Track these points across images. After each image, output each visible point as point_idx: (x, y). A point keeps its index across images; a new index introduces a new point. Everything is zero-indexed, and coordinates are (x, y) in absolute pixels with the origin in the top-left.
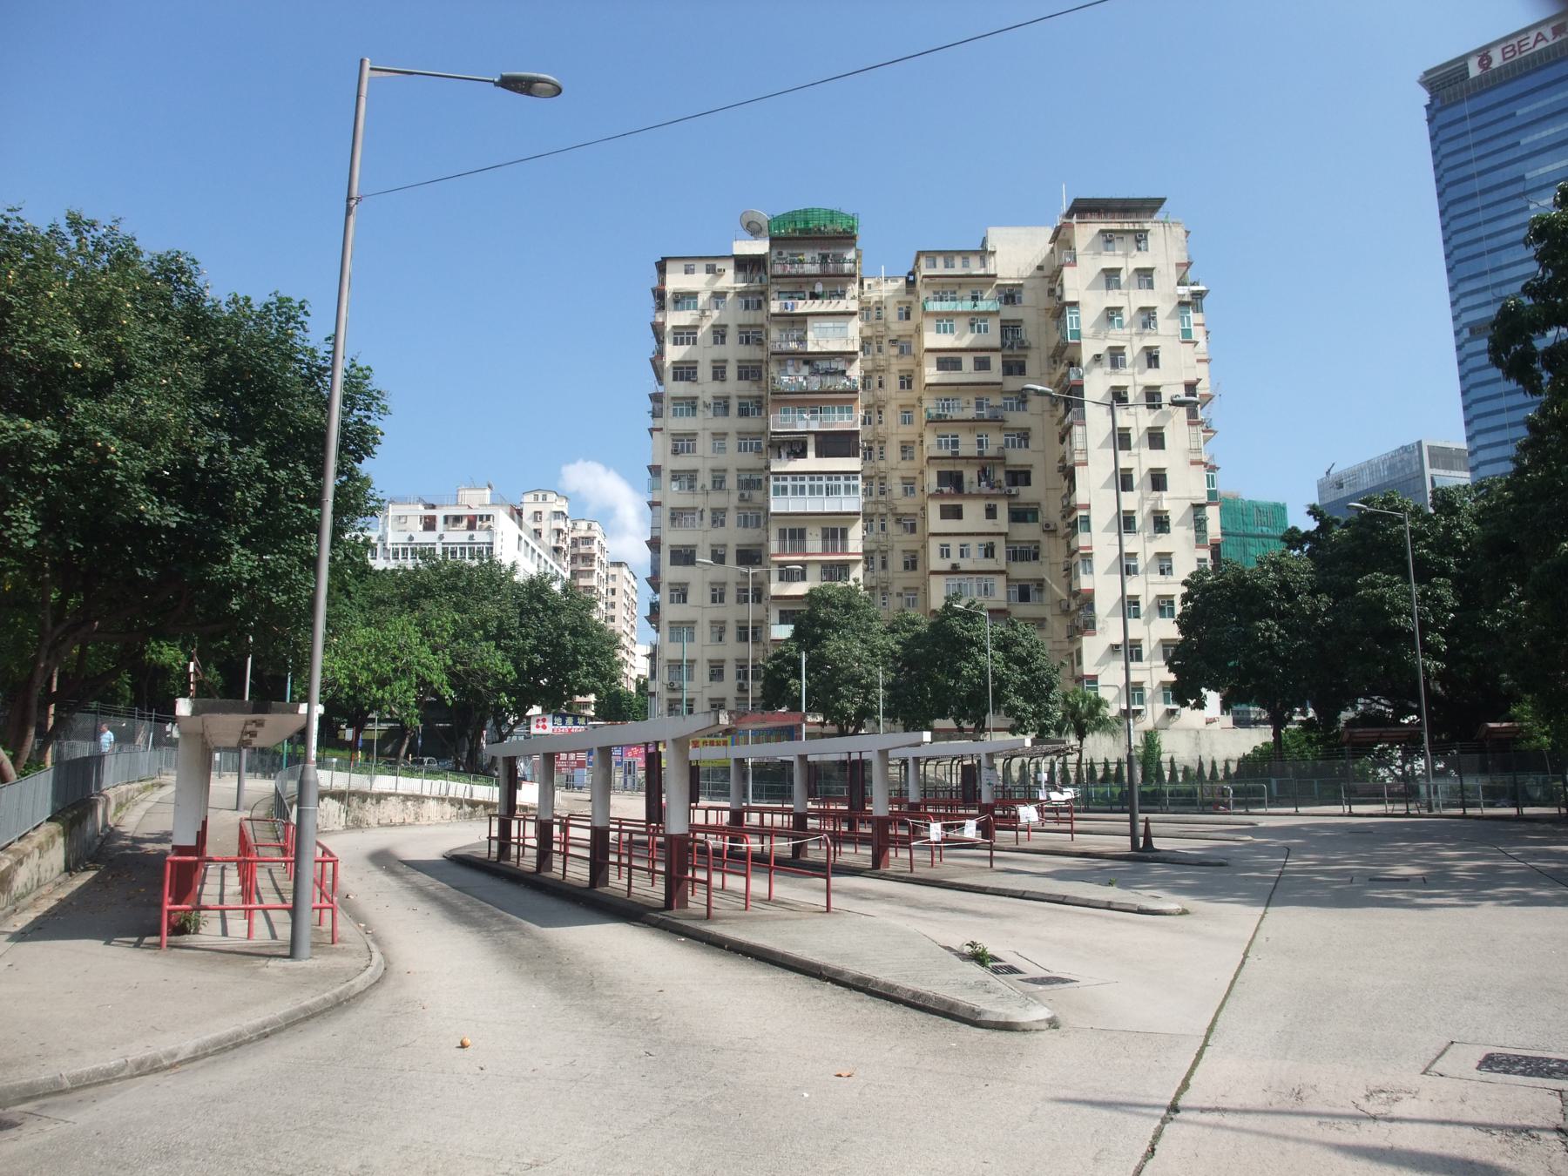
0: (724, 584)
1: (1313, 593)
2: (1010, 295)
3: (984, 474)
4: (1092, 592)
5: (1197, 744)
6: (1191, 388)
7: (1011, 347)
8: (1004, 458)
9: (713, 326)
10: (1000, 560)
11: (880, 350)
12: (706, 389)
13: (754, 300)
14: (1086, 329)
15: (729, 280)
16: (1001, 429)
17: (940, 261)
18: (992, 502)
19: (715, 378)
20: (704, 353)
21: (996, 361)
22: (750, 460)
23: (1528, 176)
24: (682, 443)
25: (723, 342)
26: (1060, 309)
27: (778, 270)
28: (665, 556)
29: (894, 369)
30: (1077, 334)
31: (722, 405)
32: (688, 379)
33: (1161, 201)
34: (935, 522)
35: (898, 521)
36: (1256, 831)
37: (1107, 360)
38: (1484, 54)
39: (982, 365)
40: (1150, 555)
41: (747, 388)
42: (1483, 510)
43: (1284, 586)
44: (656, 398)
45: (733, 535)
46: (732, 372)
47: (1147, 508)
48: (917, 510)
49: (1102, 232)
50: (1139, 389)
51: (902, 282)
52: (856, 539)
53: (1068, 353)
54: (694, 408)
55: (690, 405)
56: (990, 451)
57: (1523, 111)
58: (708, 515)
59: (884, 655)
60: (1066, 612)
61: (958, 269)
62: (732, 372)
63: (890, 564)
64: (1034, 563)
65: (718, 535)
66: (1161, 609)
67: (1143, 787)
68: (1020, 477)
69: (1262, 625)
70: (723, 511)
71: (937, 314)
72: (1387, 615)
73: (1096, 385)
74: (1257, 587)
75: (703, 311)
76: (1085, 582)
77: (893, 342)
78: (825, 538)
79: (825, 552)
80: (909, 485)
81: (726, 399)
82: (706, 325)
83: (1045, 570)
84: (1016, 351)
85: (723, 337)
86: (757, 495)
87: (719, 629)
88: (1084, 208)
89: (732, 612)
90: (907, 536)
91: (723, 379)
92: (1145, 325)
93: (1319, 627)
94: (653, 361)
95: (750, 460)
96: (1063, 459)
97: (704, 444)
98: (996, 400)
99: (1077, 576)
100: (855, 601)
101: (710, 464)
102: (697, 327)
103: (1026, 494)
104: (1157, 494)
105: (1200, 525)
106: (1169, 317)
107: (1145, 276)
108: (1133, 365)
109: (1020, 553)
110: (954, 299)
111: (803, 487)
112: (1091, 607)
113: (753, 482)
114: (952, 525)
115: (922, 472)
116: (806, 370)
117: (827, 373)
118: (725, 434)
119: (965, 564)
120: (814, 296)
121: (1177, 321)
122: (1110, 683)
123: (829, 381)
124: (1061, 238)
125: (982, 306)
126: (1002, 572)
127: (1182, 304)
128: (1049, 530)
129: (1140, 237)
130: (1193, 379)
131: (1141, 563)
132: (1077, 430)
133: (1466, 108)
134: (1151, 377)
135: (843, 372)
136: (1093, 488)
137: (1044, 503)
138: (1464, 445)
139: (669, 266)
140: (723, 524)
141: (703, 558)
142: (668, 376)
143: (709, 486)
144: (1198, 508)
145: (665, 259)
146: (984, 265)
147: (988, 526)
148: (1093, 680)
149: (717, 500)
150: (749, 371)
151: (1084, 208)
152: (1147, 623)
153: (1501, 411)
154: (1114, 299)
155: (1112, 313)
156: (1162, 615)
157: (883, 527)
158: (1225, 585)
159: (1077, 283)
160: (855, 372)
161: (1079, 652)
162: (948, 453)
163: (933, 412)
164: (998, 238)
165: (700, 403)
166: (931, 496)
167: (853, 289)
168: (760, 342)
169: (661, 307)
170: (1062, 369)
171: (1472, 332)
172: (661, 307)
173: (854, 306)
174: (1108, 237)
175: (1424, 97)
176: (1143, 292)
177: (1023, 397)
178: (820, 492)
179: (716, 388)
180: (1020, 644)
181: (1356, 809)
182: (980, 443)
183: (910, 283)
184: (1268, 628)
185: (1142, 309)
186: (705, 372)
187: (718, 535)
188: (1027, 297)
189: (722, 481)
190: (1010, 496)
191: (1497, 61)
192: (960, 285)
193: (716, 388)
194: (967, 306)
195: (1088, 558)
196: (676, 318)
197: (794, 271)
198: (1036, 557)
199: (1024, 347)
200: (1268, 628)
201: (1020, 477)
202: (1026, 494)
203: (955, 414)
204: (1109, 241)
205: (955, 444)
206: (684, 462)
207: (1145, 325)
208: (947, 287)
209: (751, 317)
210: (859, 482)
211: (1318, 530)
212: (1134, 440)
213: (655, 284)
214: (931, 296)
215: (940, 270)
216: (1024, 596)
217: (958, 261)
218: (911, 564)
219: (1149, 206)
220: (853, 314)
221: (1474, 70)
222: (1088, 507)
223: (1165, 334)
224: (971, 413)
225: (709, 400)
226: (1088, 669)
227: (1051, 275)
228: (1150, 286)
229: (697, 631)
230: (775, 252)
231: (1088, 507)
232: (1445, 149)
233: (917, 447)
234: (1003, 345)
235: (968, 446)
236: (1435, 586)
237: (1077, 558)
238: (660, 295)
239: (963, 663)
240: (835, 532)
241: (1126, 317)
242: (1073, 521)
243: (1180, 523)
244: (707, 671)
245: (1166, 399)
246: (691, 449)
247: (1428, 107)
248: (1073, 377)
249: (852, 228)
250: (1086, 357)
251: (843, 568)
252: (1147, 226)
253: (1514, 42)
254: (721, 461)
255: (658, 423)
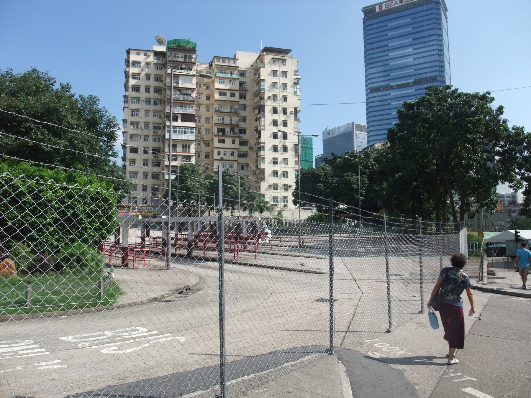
0: (148, 160)
1: (332, 177)
2: (242, 74)
3: (232, 130)
4: (264, 169)
5: (293, 215)
6: (296, 109)
7: (242, 90)
8: (238, 125)
9: (146, 74)
10: (236, 157)
11: (200, 87)
12: (143, 95)
13: (161, 66)
14: (266, 88)
15: (152, 59)
16: (238, 116)
17: (221, 60)
18: (234, 139)
19: (146, 91)
20: (143, 83)
21: (237, 94)
22: (157, 120)
23: (390, 45)
24: (135, 113)
25: (149, 80)
26: (259, 81)
27: (170, 59)
28: (128, 150)
29: (204, 93)
30: (264, 89)
31: (148, 101)
32: (137, 91)
33: (291, 50)
34: (216, 144)
35: (204, 142)
36: (318, 240)
37: (272, 98)
38: (380, 5)
39: (233, 95)
40: (281, 159)
41: (157, 96)
42: (376, 157)
43: (325, 175)
44: (125, 97)
45: (151, 144)
46: (152, 90)
47: (281, 144)
48: (210, 139)
49: (273, 58)
50: (281, 108)
51: (208, 65)
52: (193, 149)
53: (260, 95)
54: (139, 101)
55: (137, 100)
56: (234, 123)
57: (391, 24)
58: (143, 137)
59: (205, 186)
60: (255, 174)
61: (226, 64)
62: (152, 90)
63: (201, 156)
64: (246, 158)
65: (146, 144)
66: (284, 175)
67: (282, 228)
68: (243, 131)
69: (319, 185)
70: (148, 136)
71: (219, 77)
72: (351, 184)
73: (268, 106)
74: (318, 174)
75: (143, 69)
76: (262, 166)
77: (204, 85)
78: (183, 147)
79: (183, 152)
80: (208, 131)
81: (150, 99)
82: (143, 73)
83: (250, 161)
84: (243, 92)
85: (149, 78)
86: (159, 132)
87: (146, 175)
88: (267, 50)
89: (150, 169)
90: (206, 148)
91: (149, 92)
92: (284, 89)
93: (333, 186)
94: (125, 84)
95: (157, 120)
96: (256, 127)
97: (142, 113)
98: (237, 107)
99: (260, 164)
100: (195, 169)
101: (144, 120)
102: (140, 74)
103: (244, 137)
104: (284, 140)
105: (296, 151)
106: (291, 87)
107: (285, 73)
108: (280, 100)
109: (243, 155)
110: (225, 73)
111: (176, 131)
112: (264, 173)
113: (159, 128)
114: (221, 145)
115: (212, 128)
116: (178, 93)
117: (185, 94)
118: (149, 111)
119: (225, 158)
120: (182, 69)
121: (293, 88)
122: (269, 195)
123: (186, 97)
124: (260, 59)
125: (234, 76)
126: (236, 161)
127: (295, 83)
128: (251, 148)
129: (284, 61)
130: (297, 106)
131: (279, 161)
132: (262, 119)
133: (374, 21)
134: (285, 105)
135: (190, 95)
136: (266, 137)
137: (250, 140)
138: (366, 125)
139: (131, 52)
140: (148, 140)
141: (141, 151)
142: (130, 89)
143: (143, 127)
144: (296, 145)
145: (130, 49)
146: (235, 63)
147: (233, 146)
148: (264, 195)
149: (146, 132)
150: (157, 90)
151: (267, 50)
152: (280, 179)
153: (376, 116)
154: (275, 80)
155: (274, 84)
156: (284, 177)
157: (199, 144)
158: (309, 173)
159: (264, 73)
160: (194, 95)
161: (260, 187)
162: (221, 122)
163: (217, 109)
164: (240, 55)
165: (141, 99)
166: (215, 136)
167: (194, 68)
168: (162, 81)
169: (128, 65)
170: (258, 99)
171: (371, 91)
172: (128, 65)
173: (195, 73)
174: (274, 60)
175: (362, 15)
176: (284, 78)
177: (245, 107)
178: (182, 133)
179: (146, 95)
180: (246, 185)
181: (342, 235)
182: (231, 120)
183: (211, 66)
184: (320, 186)
185: (283, 84)
186: (143, 89)
187: (146, 144)
188: (247, 74)
189: (148, 126)
190: (239, 137)
191: (384, 8)
192: (227, 69)
193: (146, 95)
194: (229, 76)
195: (263, 159)
196: (133, 70)
197: (175, 60)
198: (246, 156)
199: (246, 90)
200: (320, 186)
201: (243, 131)
202: (244, 137)
203: (224, 110)
204: (275, 61)
205: (223, 119)
206: (135, 119)
207: (284, 89)
208: (222, 69)
209: (159, 72)
210: (194, 131)
211: (333, 159)
212: (279, 123)
213: (126, 57)
214: (218, 71)
215: (221, 63)
216: (242, 168)
217: (227, 61)
218: (207, 156)
219: (286, 52)
220: (194, 76)
221: (377, 10)
222: (264, 143)
223: (289, 92)
224: (228, 110)
225: (144, 99)
226: (262, 192)
227: (256, 70)
228: (286, 77)
229: (138, 175)
230: (169, 52)
231: (264, 143)
232: (368, 37)
233: (211, 120)
234: (240, 89)
235: (227, 120)
236: (363, 177)
237: (260, 158)
238: (127, 61)
239: (229, 190)
240: (186, 146)
241: (278, 85)
242: (259, 147)
243: (290, 150)
244: (141, 188)
245: (288, 112)
246: (137, 115)
247: (363, 19)
248: (262, 103)
249: (195, 47)
250: (266, 97)
251: (189, 158)
252: (286, 58)
253: (389, 3)
254: (147, 119)
255: (126, 105)
